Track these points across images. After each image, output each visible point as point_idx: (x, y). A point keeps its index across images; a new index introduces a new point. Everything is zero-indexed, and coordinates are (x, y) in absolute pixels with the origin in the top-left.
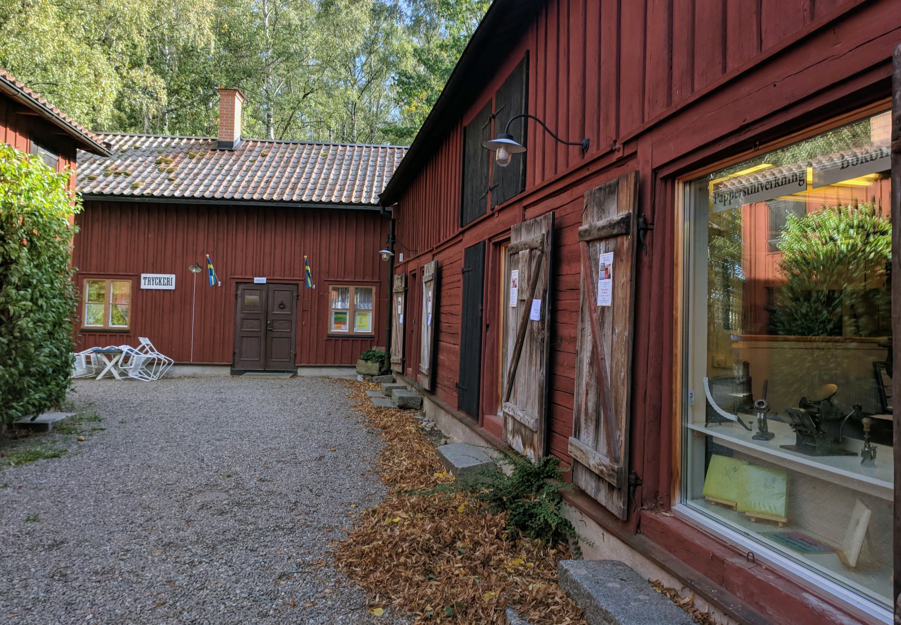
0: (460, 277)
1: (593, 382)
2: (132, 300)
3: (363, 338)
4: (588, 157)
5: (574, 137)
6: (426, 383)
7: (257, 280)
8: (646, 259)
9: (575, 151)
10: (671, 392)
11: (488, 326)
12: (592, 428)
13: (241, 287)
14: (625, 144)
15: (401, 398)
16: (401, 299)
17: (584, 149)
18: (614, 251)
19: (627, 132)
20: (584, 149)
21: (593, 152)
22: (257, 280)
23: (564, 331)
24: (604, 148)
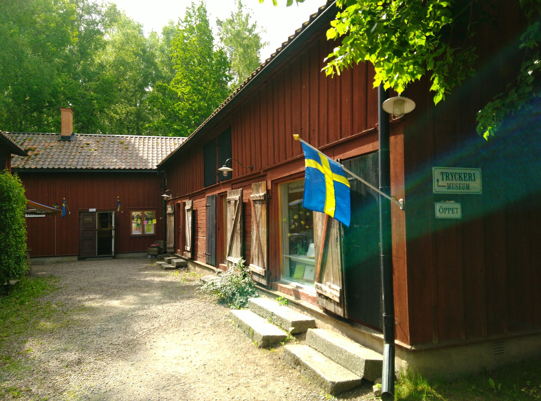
0: (205, 208)
1: (257, 245)
2: (196, 222)
3: (150, 236)
4: (253, 172)
5: (248, 166)
6: (189, 255)
7: (91, 210)
8: (270, 207)
9: (249, 170)
10: (279, 246)
11: (219, 228)
12: (257, 259)
13: (82, 214)
14: (264, 171)
15: (177, 263)
16: (172, 218)
17: (252, 169)
18: (395, 55)
19: (265, 167)
20: (252, 169)
21: (254, 171)
22: (91, 210)
23: (248, 229)
24: (258, 171)
